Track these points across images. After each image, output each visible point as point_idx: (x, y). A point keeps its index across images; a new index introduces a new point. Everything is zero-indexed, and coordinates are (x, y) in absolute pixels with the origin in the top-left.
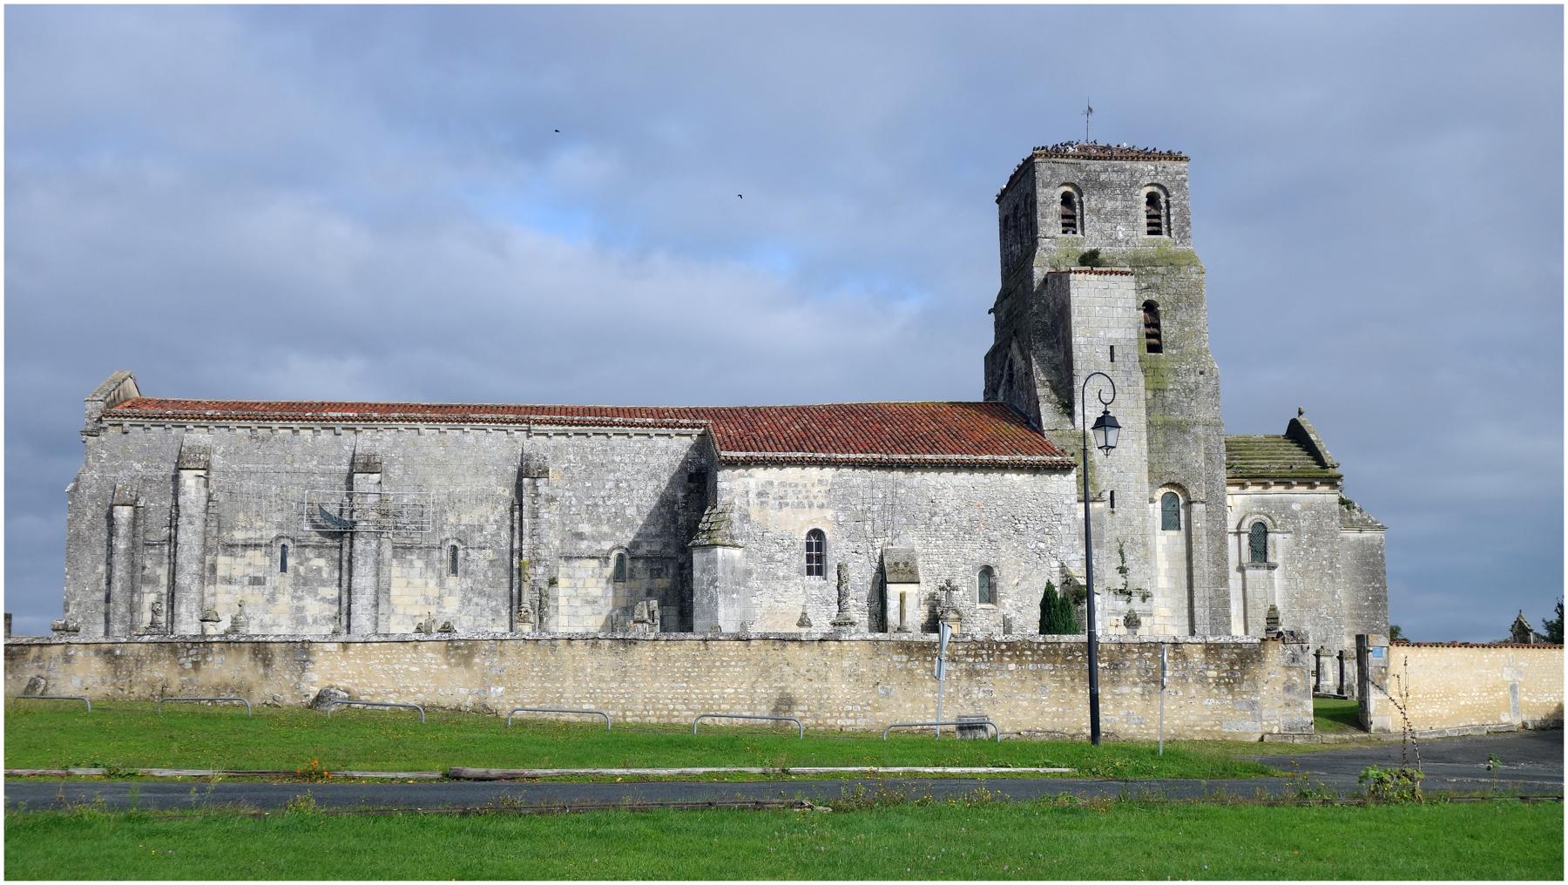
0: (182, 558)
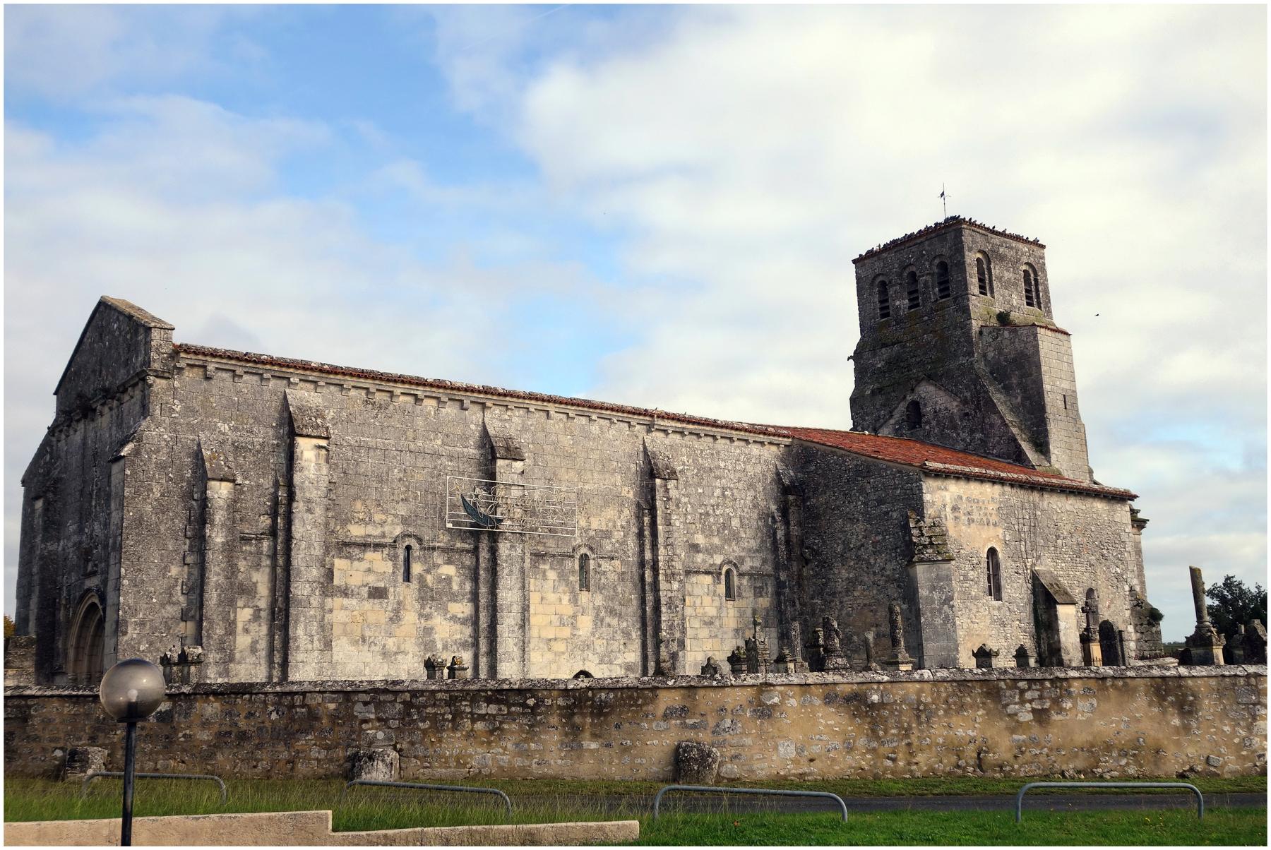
0: (298, 559)
